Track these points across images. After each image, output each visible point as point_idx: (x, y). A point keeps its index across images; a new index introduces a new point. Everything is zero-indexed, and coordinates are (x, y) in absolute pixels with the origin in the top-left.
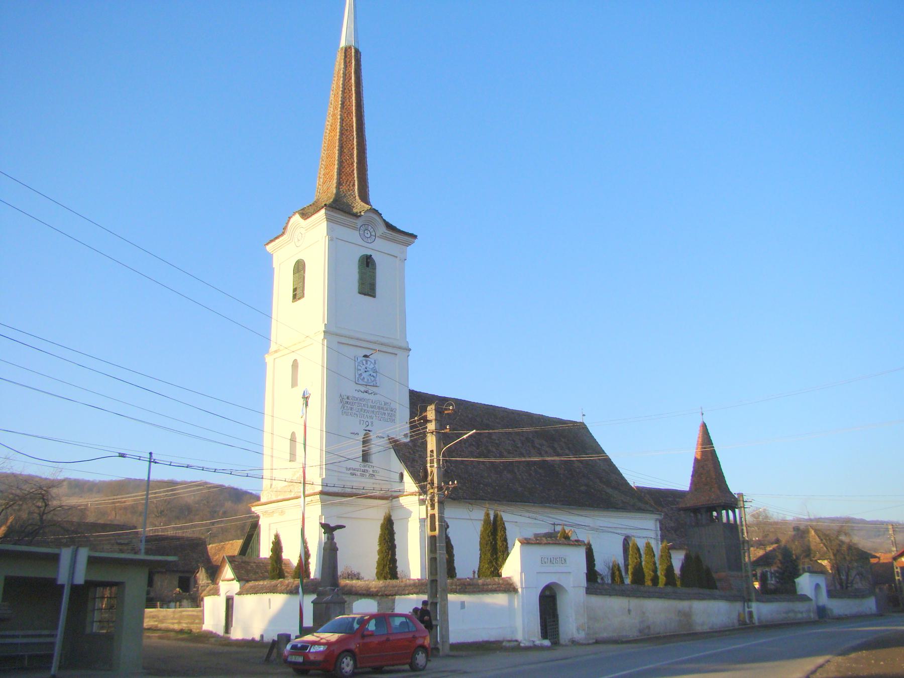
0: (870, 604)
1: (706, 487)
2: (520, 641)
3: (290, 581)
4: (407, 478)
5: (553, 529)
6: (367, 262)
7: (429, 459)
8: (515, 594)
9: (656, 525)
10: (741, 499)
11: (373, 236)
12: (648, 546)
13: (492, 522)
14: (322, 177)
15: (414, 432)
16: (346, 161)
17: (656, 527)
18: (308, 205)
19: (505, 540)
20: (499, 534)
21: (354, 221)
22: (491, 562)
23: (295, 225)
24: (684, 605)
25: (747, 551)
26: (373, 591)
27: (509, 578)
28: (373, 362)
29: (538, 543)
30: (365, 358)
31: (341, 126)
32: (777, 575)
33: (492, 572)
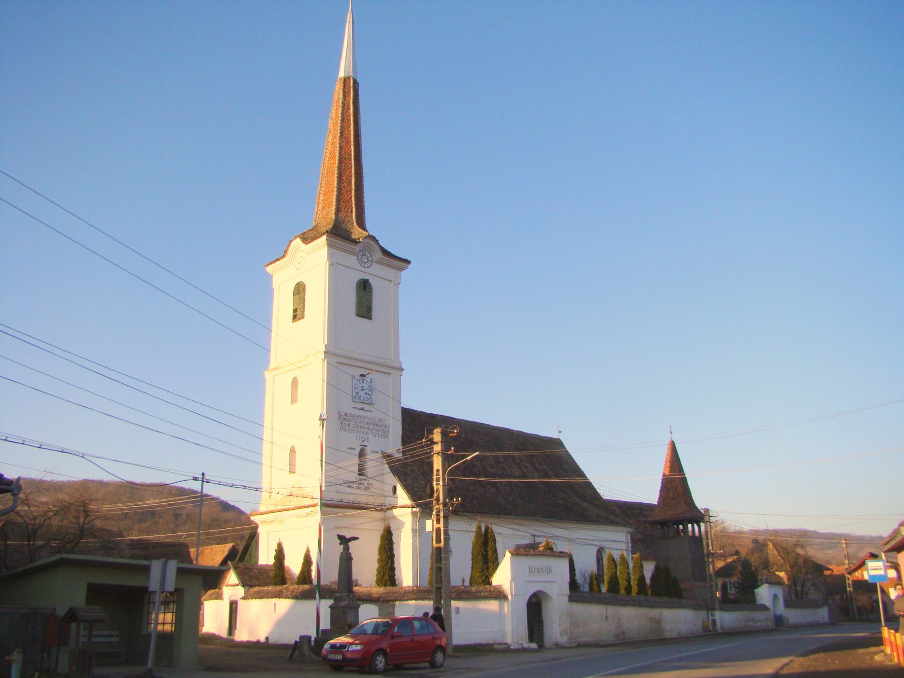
0: (823, 614)
3: (295, 587)
4: (400, 491)
5: (533, 540)
6: (364, 286)
7: (435, 477)
8: (506, 600)
9: (627, 538)
10: (707, 514)
12: (622, 557)
13: (483, 533)
14: (322, 203)
15: (405, 448)
16: (345, 188)
17: (627, 540)
19: (496, 551)
21: (354, 247)
22: (483, 571)
24: (655, 612)
25: (712, 563)
26: (375, 597)
27: (500, 586)
28: (369, 381)
29: (527, 555)
30: (361, 377)
31: (340, 154)
32: (736, 585)
33: (483, 581)
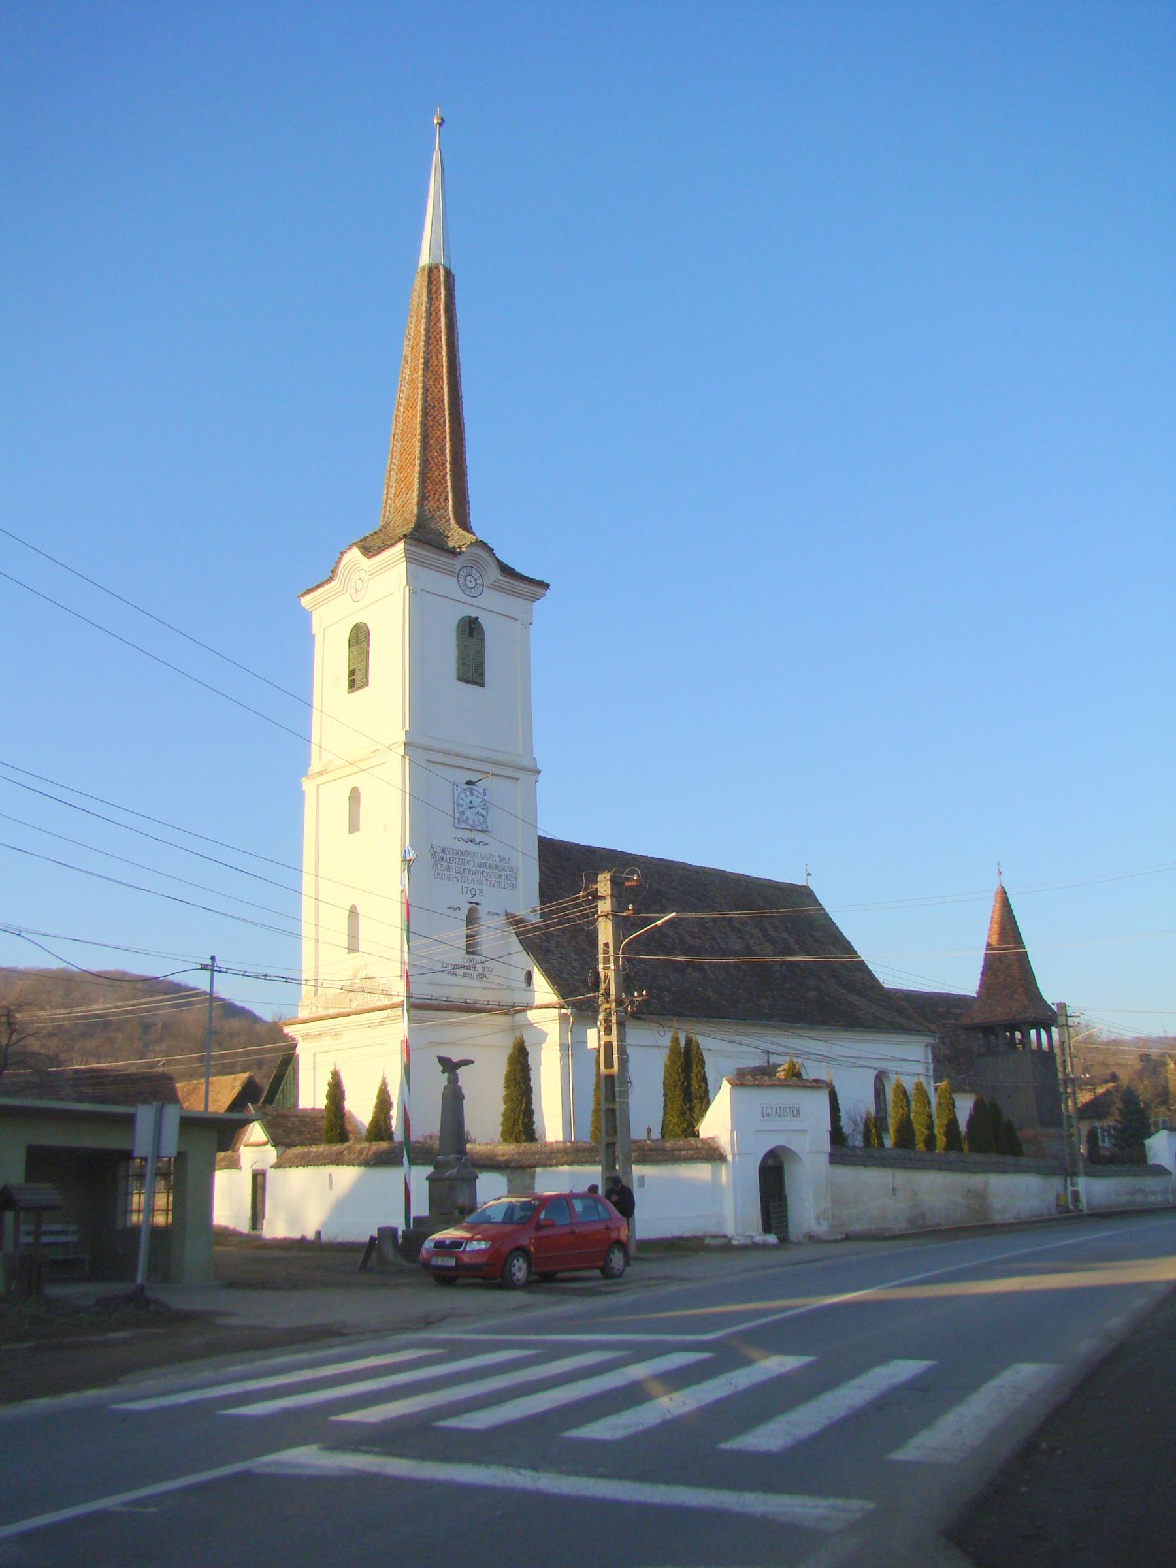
1: (1005, 992)
2: (729, 1236)
3: (363, 1145)
4: (539, 979)
6: (471, 629)
7: (601, 956)
9: (926, 1053)
11: (479, 585)
16: (434, 460)
17: (926, 1058)
18: (371, 533)
20: (695, 1071)
21: (451, 562)
22: (683, 1114)
23: (351, 566)
25: (1072, 1095)
26: (500, 1161)
29: (758, 1085)
30: (468, 786)
33: (684, 1131)
